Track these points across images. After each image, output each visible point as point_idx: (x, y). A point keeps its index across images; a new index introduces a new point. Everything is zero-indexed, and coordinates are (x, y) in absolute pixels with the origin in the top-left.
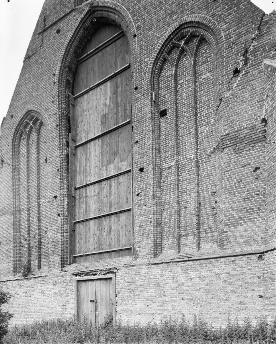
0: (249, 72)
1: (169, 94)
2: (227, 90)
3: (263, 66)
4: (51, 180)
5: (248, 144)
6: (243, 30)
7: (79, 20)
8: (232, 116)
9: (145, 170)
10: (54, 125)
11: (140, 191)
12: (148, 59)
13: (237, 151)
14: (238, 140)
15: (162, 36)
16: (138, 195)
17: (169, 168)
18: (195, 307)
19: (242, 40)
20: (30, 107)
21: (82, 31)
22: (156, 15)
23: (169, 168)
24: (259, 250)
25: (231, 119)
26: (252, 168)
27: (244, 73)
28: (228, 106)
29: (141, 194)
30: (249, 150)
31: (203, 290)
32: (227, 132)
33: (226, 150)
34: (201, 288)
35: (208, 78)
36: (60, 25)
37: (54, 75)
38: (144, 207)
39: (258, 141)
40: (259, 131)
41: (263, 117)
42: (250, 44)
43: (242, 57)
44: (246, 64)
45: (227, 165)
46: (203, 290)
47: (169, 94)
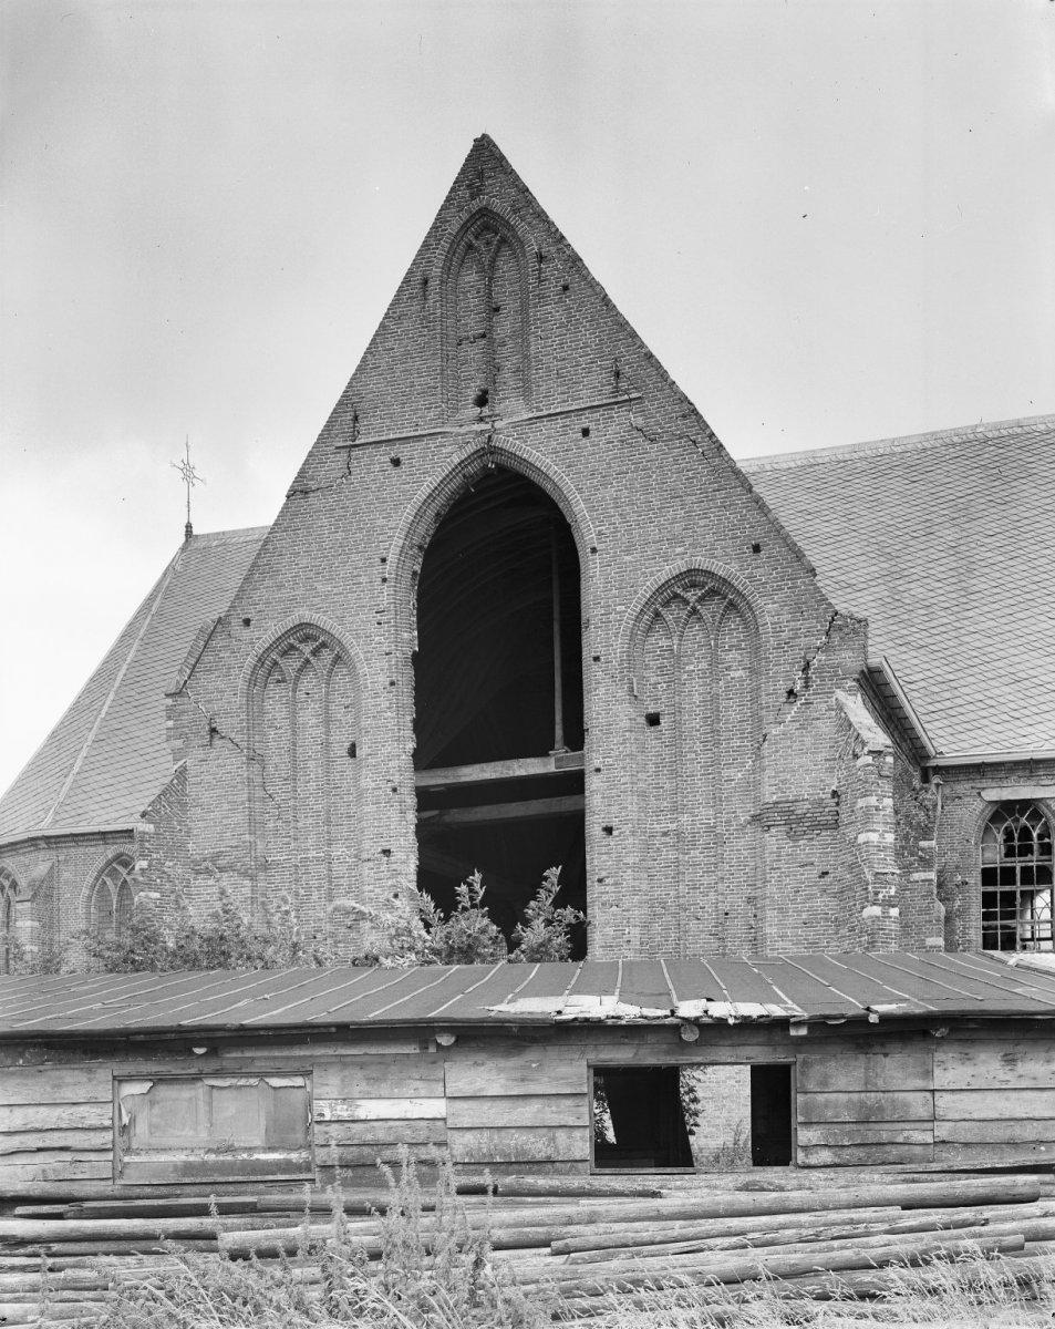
0: (812, 703)
1: (665, 685)
2: (776, 723)
3: (834, 699)
4: (373, 808)
5: (812, 828)
6: (803, 625)
7: (457, 461)
8: (784, 771)
9: (615, 833)
10: (383, 679)
11: (604, 874)
12: (623, 608)
13: (792, 836)
14: (794, 817)
15: (652, 574)
16: (600, 881)
17: (665, 834)
18: (718, 1113)
19: (803, 641)
20: (304, 614)
21: (459, 480)
22: (641, 528)
23: (665, 834)
24: (460, 1090)
25: (782, 776)
26: (816, 872)
27: (803, 701)
28: (777, 752)
29: (607, 881)
30: (812, 839)
31: (733, 1082)
32: (775, 797)
33: (773, 830)
34: (729, 1078)
35: (741, 680)
36: (403, 451)
37: (384, 560)
38: (614, 908)
39: (826, 826)
40: (827, 810)
41: (834, 788)
42: (813, 655)
43: (800, 673)
44: (807, 687)
45: (774, 857)
46: (733, 1082)
47: (665, 685)
